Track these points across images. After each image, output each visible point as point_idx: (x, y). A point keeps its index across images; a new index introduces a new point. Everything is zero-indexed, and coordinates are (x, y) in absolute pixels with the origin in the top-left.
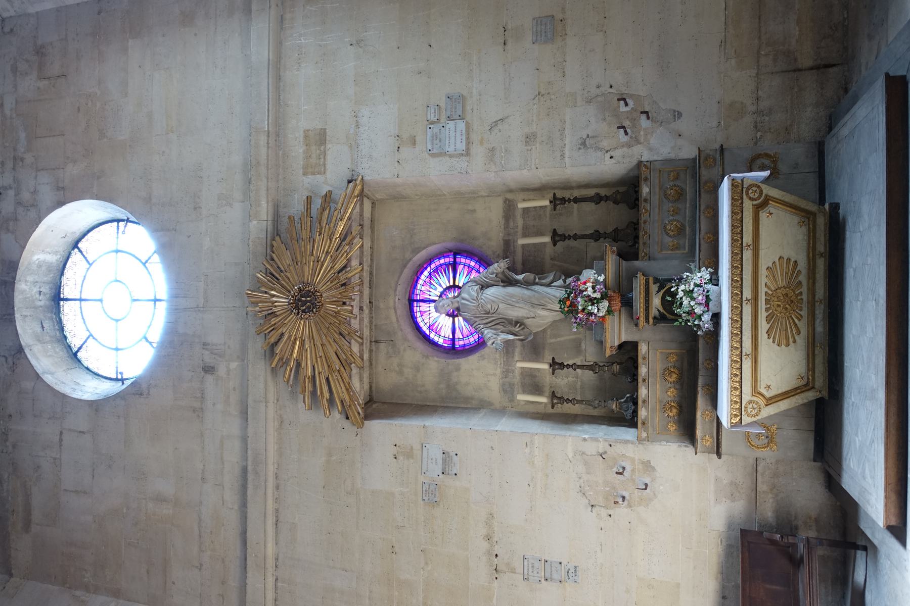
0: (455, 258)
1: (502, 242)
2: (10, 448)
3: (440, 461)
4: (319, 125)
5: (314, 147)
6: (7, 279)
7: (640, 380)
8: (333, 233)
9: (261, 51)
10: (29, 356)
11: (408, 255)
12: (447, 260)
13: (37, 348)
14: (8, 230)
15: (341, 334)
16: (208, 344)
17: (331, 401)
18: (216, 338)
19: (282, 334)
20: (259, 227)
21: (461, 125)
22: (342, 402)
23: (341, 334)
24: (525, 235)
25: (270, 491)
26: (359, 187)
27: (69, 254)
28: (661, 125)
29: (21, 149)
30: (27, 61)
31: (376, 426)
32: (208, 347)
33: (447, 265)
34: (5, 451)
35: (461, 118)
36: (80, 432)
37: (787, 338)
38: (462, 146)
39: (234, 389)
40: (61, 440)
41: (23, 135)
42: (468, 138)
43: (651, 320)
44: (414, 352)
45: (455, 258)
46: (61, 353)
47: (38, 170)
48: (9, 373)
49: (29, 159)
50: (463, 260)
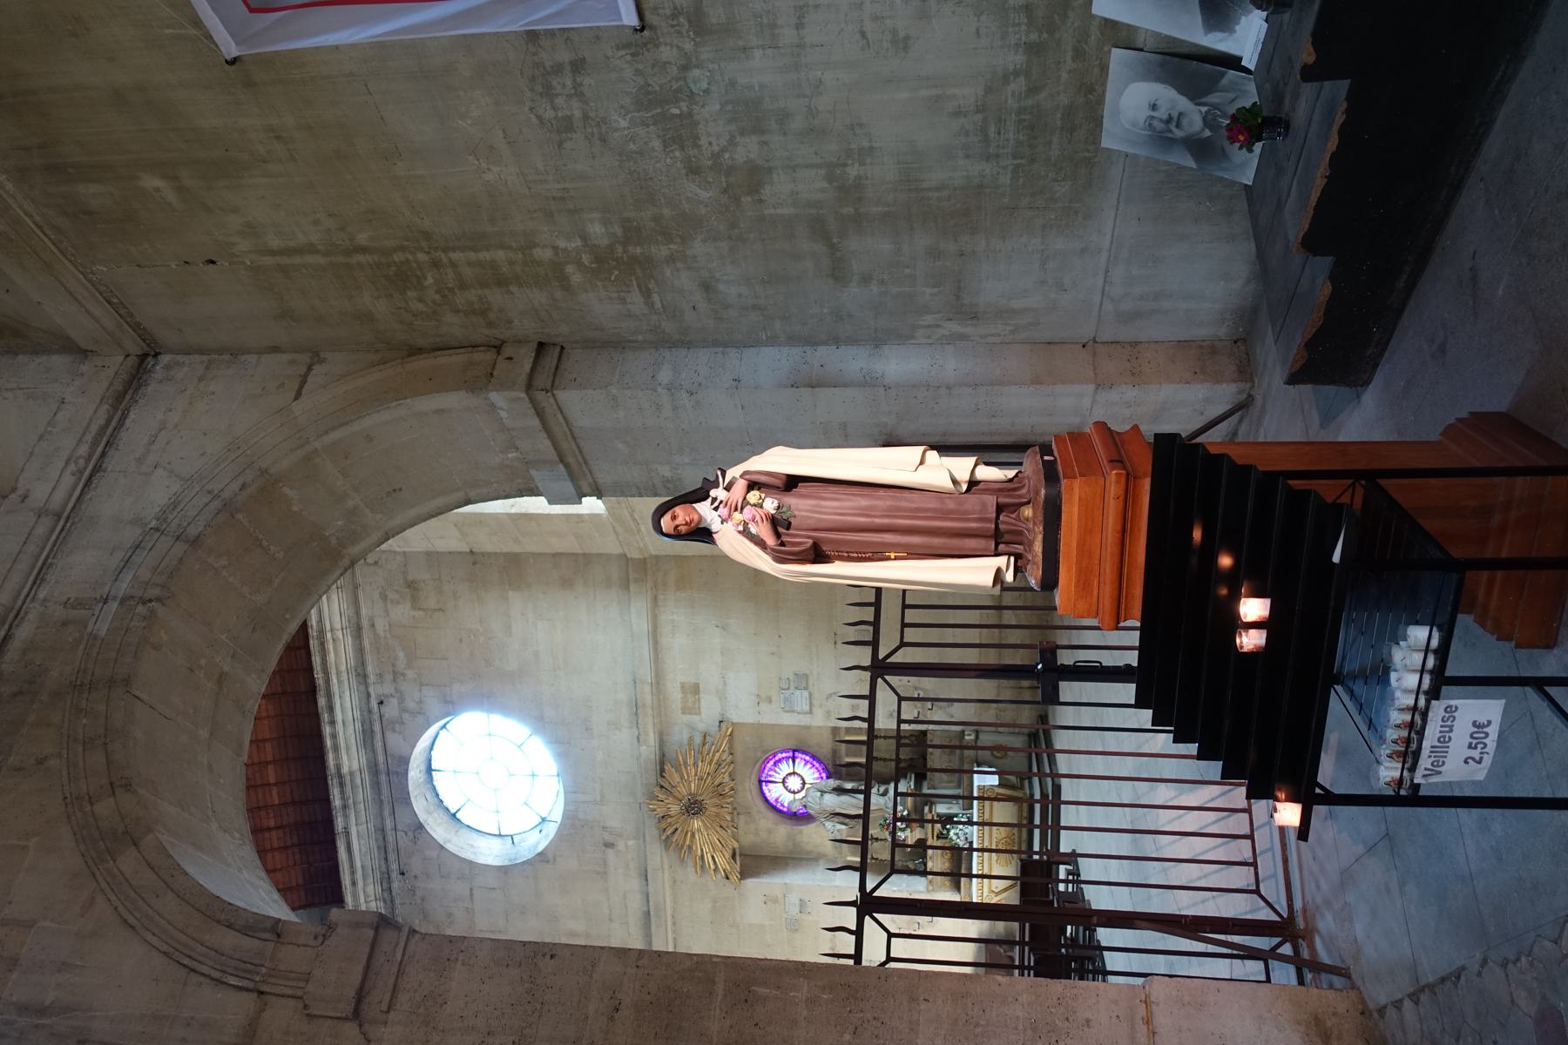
0: (794, 754)
1: (830, 751)
2: (419, 901)
3: (798, 906)
4: (693, 680)
5: (689, 696)
6: (399, 770)
7: (928, 858)
8: (711, 761)
9: (641, 624)
10: (429, 831)
11: (759, 754)
12: (788, 755)
13: (430, 821)
14: (394, 731)
15: (721, 827)
16: (607, 828)
17: (716, 869)
18: (614, 823)
19: (676, 829)
20: (649, 750)
21: (806, 694)
22: (724, 871)
23: (721, 827)
24: (847, 755)
25: (669, 923)
26: (730, 730)
27: (438, 733)
28: (870, 134)
29: (401, 664)
30: (397, 591)
31: (751, 882)
32: (609, 830)
33: (788, 758)
34: (413, 903)
35: (806, 689)
36: (491, 889)
37: (1006, 863)
38: (807, 708)
39: (633, 859)
40: (472, 895)
41: (401, 655)
42: (811, 703)
43: (935, 838)
44: (767, 820)
45: (794, 754)
46: (444, 818)
47: (421, 685)
48: (410, 844)
49: (410, 674)
50: (800, 755)
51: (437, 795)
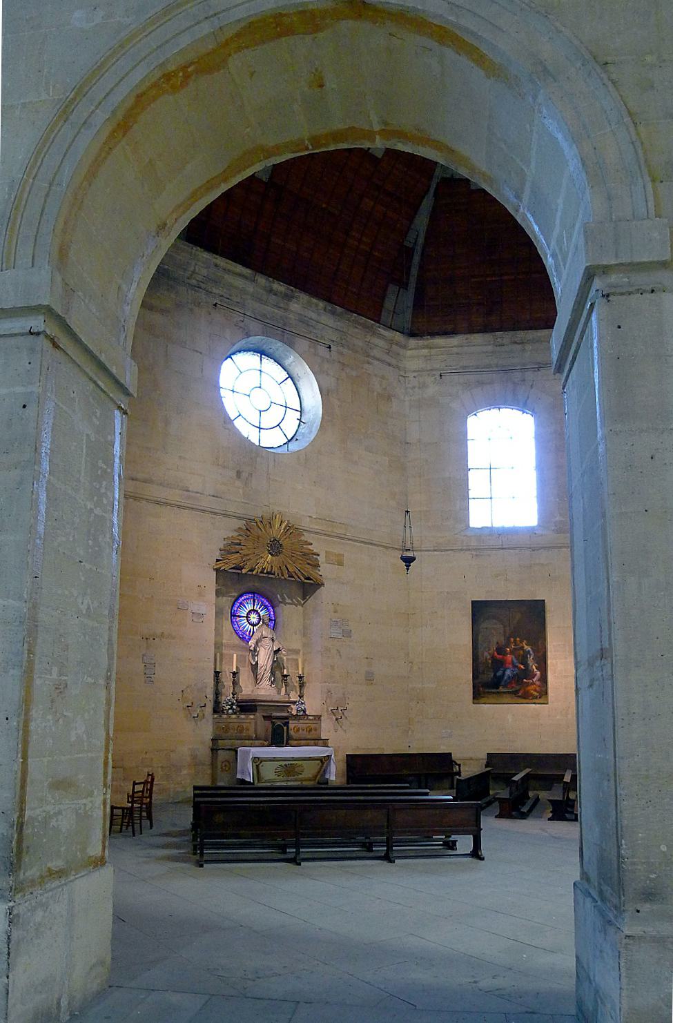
27: (286, 370)
40: (197, 351)
51: (244, 351)
